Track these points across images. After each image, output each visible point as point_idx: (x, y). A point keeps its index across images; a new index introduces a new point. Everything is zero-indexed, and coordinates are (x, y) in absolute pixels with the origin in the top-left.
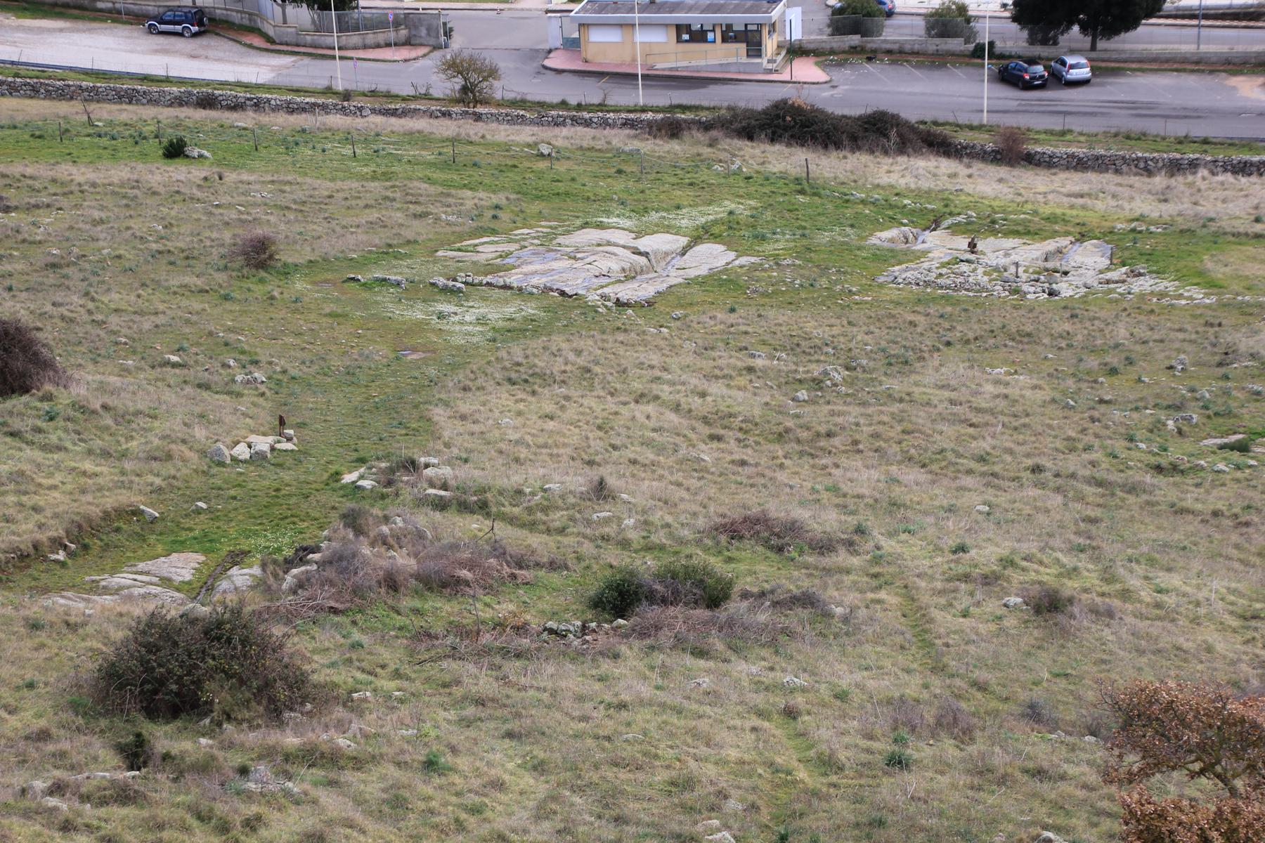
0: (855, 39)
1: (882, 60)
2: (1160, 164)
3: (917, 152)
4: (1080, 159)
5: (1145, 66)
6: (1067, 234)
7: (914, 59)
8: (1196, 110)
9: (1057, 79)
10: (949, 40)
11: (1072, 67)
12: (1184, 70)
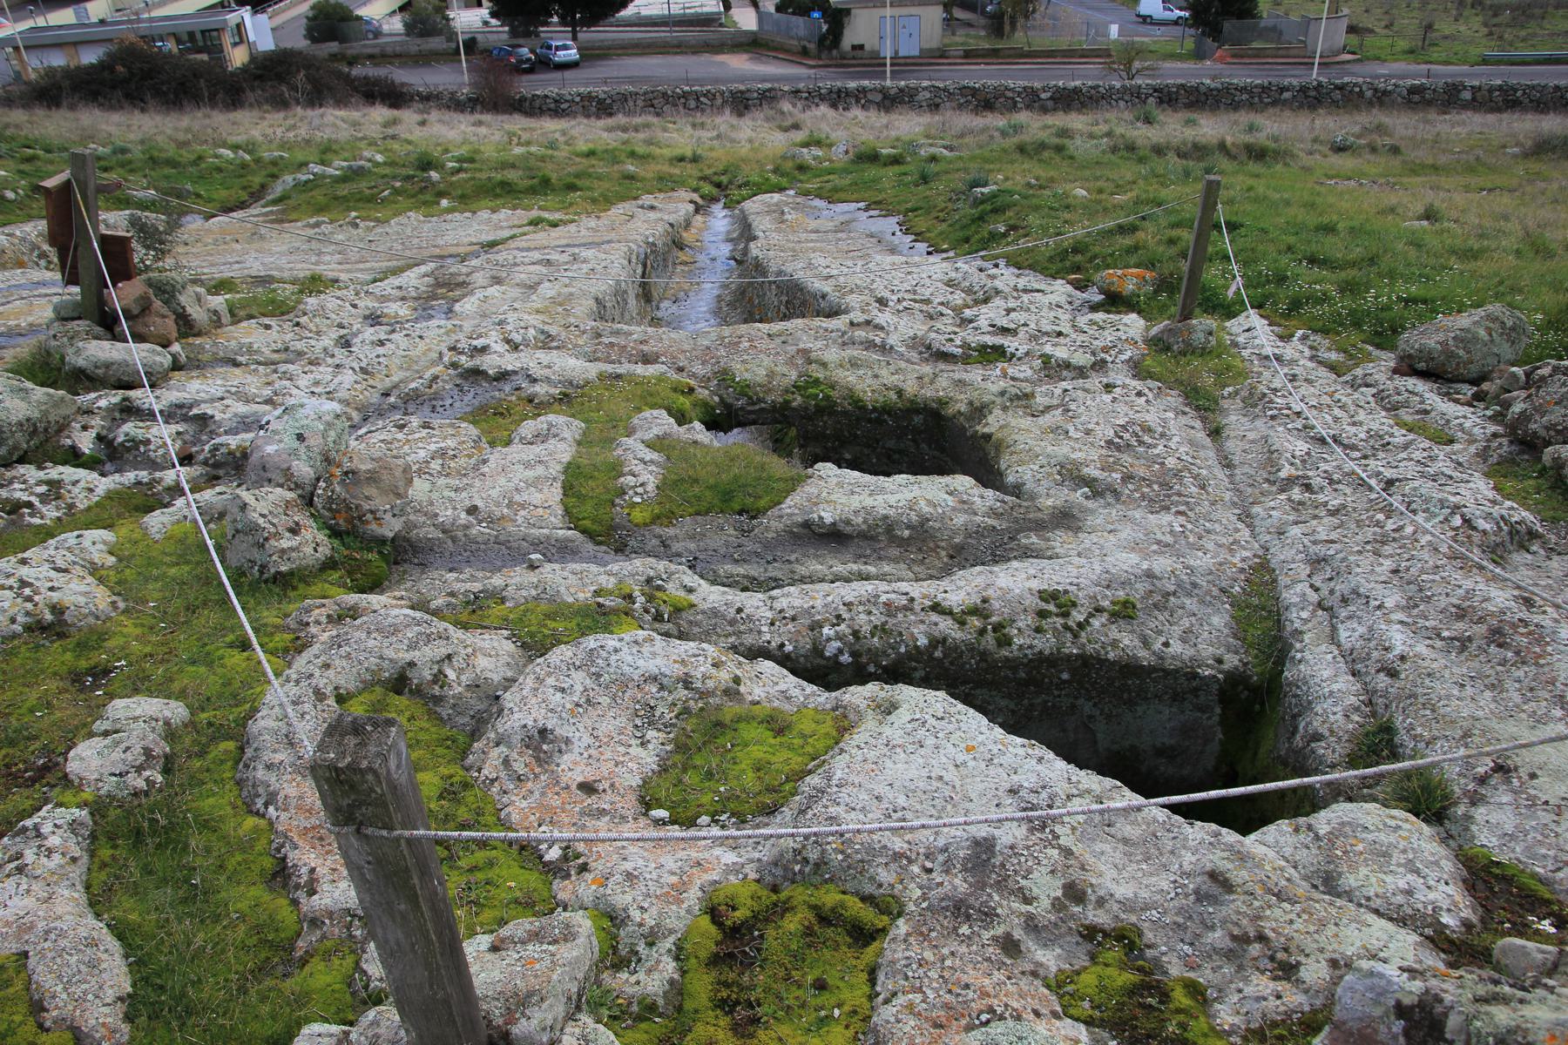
0: (333, 47)
2: (719, 101)
4: (601, 102)
6: (666, 184)
7: (397, 63)
9: (544, 64)
10: (431, 39)
11: (557, 48)
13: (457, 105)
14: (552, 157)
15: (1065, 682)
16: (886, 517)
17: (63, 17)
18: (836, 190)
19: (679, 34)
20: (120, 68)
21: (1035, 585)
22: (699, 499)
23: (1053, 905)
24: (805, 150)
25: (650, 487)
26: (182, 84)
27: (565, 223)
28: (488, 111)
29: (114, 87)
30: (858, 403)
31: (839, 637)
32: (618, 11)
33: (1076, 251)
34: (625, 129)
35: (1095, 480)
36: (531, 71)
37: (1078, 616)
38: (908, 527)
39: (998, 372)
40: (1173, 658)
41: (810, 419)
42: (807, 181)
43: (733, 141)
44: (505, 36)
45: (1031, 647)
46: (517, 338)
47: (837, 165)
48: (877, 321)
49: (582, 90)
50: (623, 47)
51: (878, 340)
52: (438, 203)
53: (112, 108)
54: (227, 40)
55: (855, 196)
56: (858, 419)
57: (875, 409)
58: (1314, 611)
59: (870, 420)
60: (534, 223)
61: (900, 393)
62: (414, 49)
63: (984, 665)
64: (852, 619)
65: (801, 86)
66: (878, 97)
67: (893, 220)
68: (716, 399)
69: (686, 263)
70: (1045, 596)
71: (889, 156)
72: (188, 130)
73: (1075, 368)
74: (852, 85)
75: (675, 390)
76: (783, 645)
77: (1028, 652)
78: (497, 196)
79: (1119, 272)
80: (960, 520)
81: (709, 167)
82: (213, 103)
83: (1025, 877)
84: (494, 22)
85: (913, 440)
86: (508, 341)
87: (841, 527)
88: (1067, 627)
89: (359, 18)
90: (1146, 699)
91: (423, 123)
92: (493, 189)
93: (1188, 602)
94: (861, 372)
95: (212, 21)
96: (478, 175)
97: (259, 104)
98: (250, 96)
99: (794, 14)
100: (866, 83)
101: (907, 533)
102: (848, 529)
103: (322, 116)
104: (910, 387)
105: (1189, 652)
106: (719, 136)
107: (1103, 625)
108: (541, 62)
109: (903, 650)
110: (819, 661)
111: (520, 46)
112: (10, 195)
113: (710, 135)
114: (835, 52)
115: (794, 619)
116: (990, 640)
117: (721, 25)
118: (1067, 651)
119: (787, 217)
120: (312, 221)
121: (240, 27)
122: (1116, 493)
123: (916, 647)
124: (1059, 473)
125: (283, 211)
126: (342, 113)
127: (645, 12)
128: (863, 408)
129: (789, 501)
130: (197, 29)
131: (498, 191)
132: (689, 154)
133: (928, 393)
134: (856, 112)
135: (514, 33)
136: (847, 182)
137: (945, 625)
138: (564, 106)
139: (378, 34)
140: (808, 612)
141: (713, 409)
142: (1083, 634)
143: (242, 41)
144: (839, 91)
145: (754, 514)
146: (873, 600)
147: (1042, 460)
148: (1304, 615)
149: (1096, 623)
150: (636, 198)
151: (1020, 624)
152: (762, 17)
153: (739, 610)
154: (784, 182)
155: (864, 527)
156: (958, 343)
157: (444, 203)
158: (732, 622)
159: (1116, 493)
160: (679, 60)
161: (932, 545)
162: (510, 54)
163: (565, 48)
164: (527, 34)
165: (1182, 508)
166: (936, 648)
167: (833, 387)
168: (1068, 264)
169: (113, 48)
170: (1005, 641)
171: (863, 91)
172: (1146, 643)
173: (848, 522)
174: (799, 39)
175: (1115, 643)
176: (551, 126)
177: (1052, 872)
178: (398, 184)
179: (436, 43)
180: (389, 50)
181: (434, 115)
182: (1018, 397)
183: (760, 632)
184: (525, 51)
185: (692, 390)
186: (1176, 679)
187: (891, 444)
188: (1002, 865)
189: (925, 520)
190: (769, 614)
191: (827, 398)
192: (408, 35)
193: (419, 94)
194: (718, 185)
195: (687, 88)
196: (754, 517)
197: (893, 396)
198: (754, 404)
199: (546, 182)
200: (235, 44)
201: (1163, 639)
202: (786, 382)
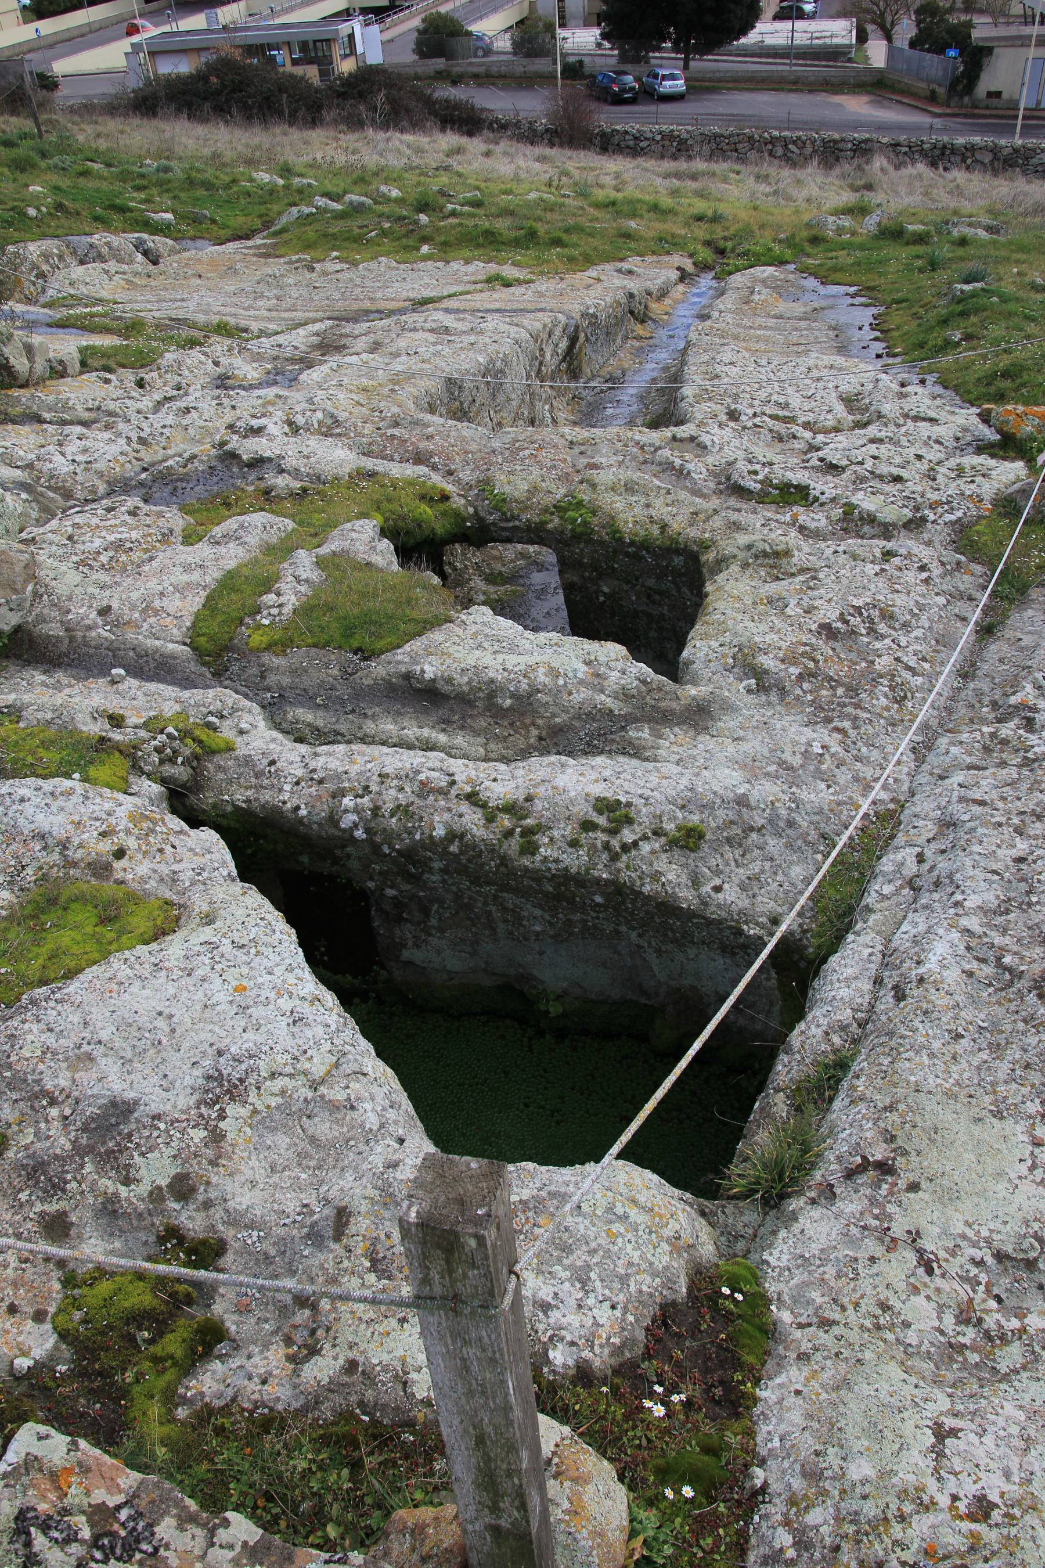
0: (440, 63)
1: (467, 85)
2: (809, 150)
3: (416, 126)
4: (682, 142)
5: (741, 86)
6: (665, 245)
7: (500, 83)
8: (806, 123)
9: (648, 95)
10: (537, 60)
11: (664, 78)
12: (782, 90)
13: (529, 135)
14: (563, 205)
15: (598, 905)
16: (492, 681)
17: (196, 21)
19: (800, 68)
20: (214, 80)
21: (599, 790)
22: (322, 628)
23: (151, 1193)
25: (287, 610)
26: (268, 98)
27: (519, 282)
28: (561, 145)
29: (206, 99)
30: (615, 532)
31: (357, 810)
32: (737, 39)
33: (1006, 374)
34: (678, 175)
35: (766, 672)
36: (633, 101)
37: (628, 835)
38: (513, 696)
39: (788, 518)
40: (719, 906)
41: (566, 544)
44: (613, 61)
45: (556, 861)
46: (300, 420)
48: (701, 439)
49: (664, 127)
50: (736, 80)
51: (678, 462)
52: (418, 249)
53: (204, 120)
54: (337, 51)
55: (853, 278)
56: (615, 551)
57: (632, 543)
58: (902, 887)
59: (627, 555)
60: (494, 281)
61: (664, 527)
62: (519, 70)
63: (503, 869)
64: (380, 793)
65: (902, 138)
66: (987, 158)
68: (471, 510)
69: (639, 338)
70: (604, 805)
71: (914, 233)
72: (259, 147)
73: (880, 524)
74: (960, 141)
75: (423, 497)
76: (298, 808)
77: (553, 866)
78: (479, 246)
79: (1021, 408)
80: (581, 695)
82: (292, 121)
83: (143, 1155)
84: (607, 44)
85: (674, 582)
86: (290, 423)
87: (440, 685)
88: (607, 846)
89: (469, 34)
90: (694, 943)
91: (488, 154)
92: (477, 237)
93: (772, 841)
94: (635, 498)
95: (325, 31)
96: (465, 222)
97: (336, 122)
98: (328, 115)
99: (929, 51)
100: (977, 139)
101: (508, 702)
102: (446, 689)
103: (388, 140)
104: (676, 525)
105: (744, 903)
106: (776, 192)
107: (653, 852)
108: (646, 92)
109: (418, 837)
110: (333, 831)
111: (625, 73)
112: (32, 212)
113: (768, 190)
114: (966, 99)
115: (321, 782)
116: (514, 844)
117: (850, 60)
118: (596, 873)
120: (294, 258)
121: (351, 37)
122: (783, 692)
123: (431, 836)
124: (734, 658)
125: (275, 246)
126: (408, 138)
127: (769, 41)
128: (621, 540)
129: (407, 647)
130: (309, 38)
131: (481, 240)
133: (693, 533)
134: (958, 175)
135: (623, 58)
136: (850, 260)
137: (472, 820)
138: (643, 144)
139: (488, 51)
140: (338, 776)
141: (464, 520)
142: (624, 858)
143: (351, 54)
144: (944, 147)
145: (366, 654)
146: (410, 776)
147: (727, 637)
148: (887, 889)
149: (645, 847)
150: (622, 260)
151: (556, 833)
152: (892, 53)
153: (273, 763)
154: (788, 254)
155: (466, 689)
156: (760, 477)
157: (425, 249)
158: (258, 775)
159: (783, 692)
160: (793, 98)
161: (528, 721)
162: (613, 81)
163: (673, 78)
164: (637, 60)
165: (846, 724)
166: (452, 842)
167: (594, 513)
168: (992, 389)
169: (205, 58)
170: (530, 848)
171: (972, 148)
172: (696, 882)
173: (449, 681)
174: (929, 81)
175: (656, 876)
176: (614, 165)
177: (175, 1157)
178: (387, 225)
179: (541, 65)
180: (494, 70)
181: (504, 145)
182: (765, 554)
183: (281, 790)
184: (629, 78)
185: (445, 498)
186: (721, 930)
187: (651, 582)
188: (130, 1135)
189: (534, 690)
190: (299, 772)
191: (585, 523)
192: (515, 54)
193: (497, 121)
195: (776, 133)
196: (366, 659)
197: (655, 530)
198: (508, 520)
199: (532, 234)
200: (346, 56)
201: (717, 882)
202: (549, 500)
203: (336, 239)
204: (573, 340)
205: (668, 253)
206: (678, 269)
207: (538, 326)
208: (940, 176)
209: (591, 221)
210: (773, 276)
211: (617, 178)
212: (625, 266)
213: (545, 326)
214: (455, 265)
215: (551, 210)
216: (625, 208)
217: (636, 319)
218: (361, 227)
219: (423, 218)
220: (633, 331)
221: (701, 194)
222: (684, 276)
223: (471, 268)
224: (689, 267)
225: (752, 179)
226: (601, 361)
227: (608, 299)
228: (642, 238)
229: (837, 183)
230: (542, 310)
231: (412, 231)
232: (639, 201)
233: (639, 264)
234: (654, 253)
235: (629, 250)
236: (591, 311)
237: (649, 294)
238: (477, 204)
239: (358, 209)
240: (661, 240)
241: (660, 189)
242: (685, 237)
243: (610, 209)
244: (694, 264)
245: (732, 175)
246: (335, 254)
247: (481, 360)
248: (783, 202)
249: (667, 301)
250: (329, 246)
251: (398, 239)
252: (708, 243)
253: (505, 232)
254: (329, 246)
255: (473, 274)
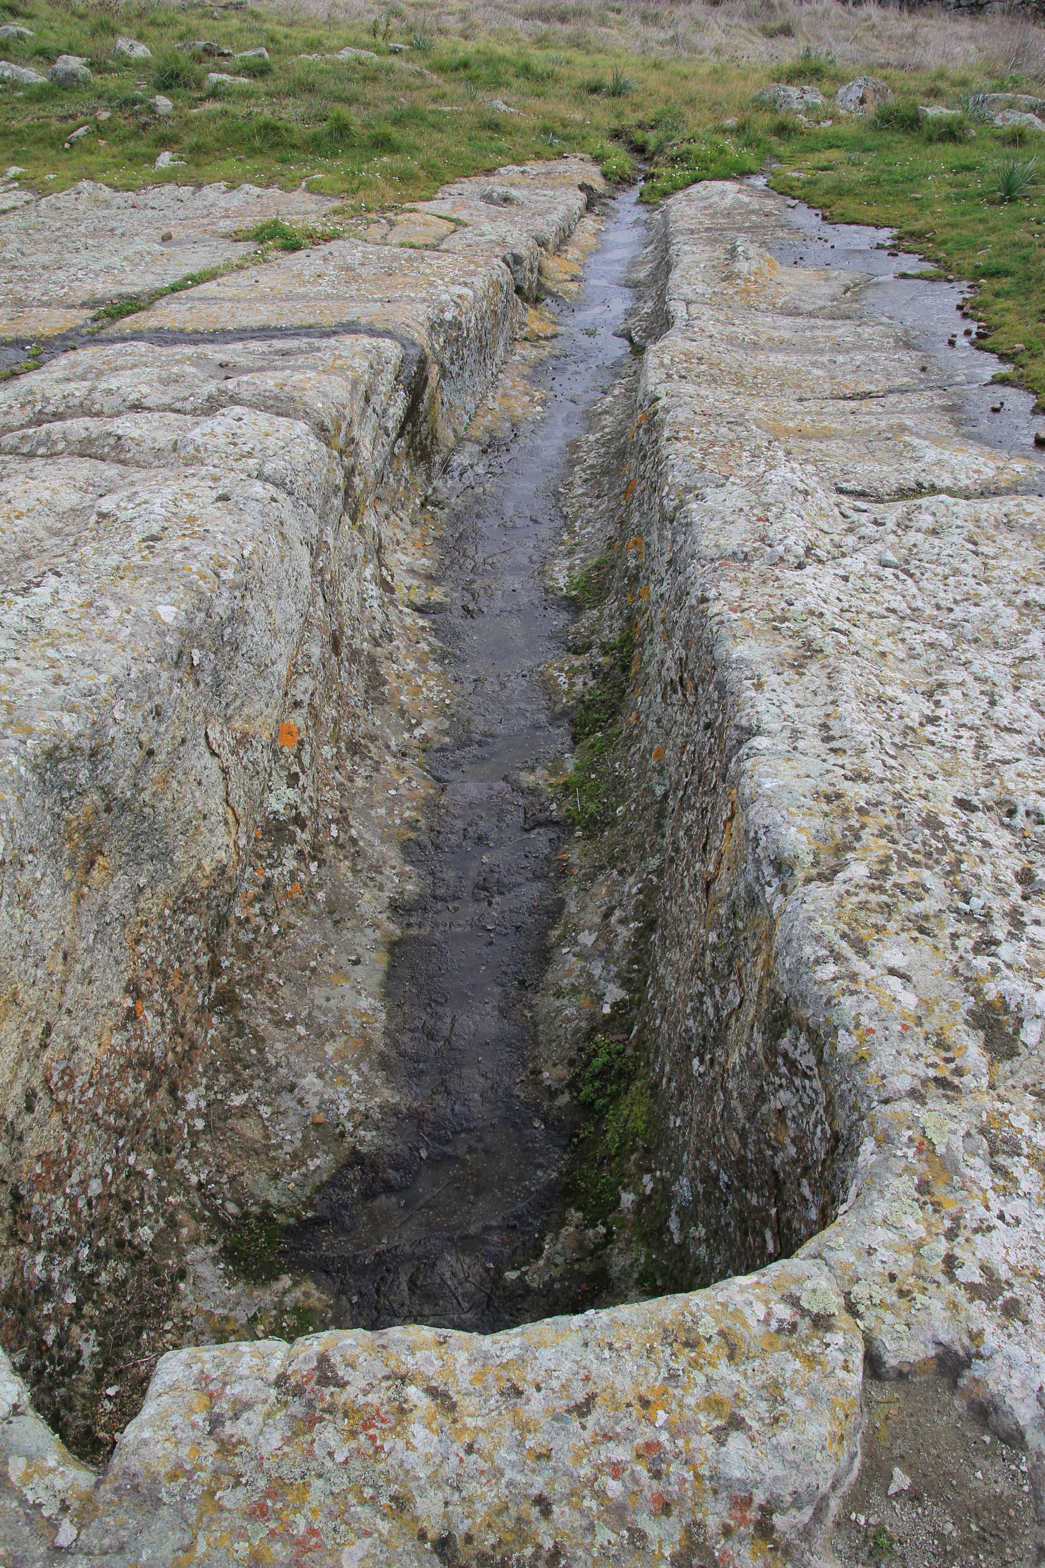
14: (390, 70)
18: (839, 191)
24: (793, 91)
42: (790, 160)
43: (694, 49)
47: (842, 129)
52: (152, 159)
67: (953, 294)
69: (533, 339)
71: (938, 123)
78: (254, 152)
81: (636, 107)
106: (674, 40)
113: (662, 36)
119: (742, 266)
131: (257, 143)
132: (609, 80)
150: (489, 172)
157: (165, 159)
194: (639, 149)
199: (342, 129)
203: (22, 141)
204: (416, 388)
205: (560, 155)
206: (582, 187)
207: (338, 389)
208: (849, 13)
209: (435, 100)
210: (742, 205)
211: (464, 19)
212: (496, 185)
213: (355, 384)
214: (211, 193)
215: (374, 79)
216: (484, 72)
217: (526, 300)
218: (63, 119)
219: (163, 103)
220: (523, 324)
221: (576, 43)
222: (593, 201)
223: (236, 200)
224: (599, 184)
225: (637, 22)
226: (471, 406)
227: (479, 282)
228: (517, 129)
229: (745, 25)
230: (351, 328)
231: (145, 126)
232: (502, 59)
233: (518, 179)
234: (538, 156)
235: (500, 152)
236: (448, 316)
237: (542, 244)
238: (259, 71)
239: (67, 83)
240: (546, 130)
241: (522, 35)
242: (582, 125)
243: (462, 74)
244: (605, 175)
245: (612, 15)
246: (14, 170)
247: (168, 613)
248: (685, 55)
249: (573, 252)
250: (9, 154)
251: (123, 140)
252: (616, 135)
253: (296, 126)
254: (9, 154)
255: (239, 214)
